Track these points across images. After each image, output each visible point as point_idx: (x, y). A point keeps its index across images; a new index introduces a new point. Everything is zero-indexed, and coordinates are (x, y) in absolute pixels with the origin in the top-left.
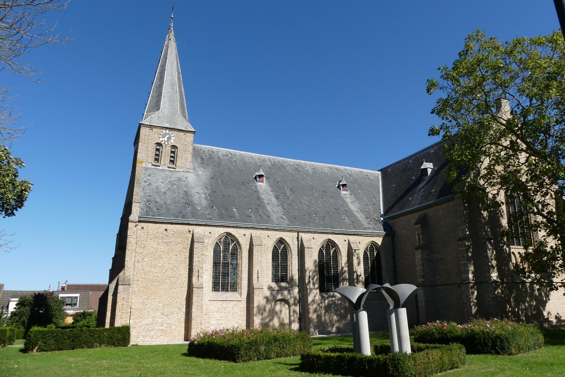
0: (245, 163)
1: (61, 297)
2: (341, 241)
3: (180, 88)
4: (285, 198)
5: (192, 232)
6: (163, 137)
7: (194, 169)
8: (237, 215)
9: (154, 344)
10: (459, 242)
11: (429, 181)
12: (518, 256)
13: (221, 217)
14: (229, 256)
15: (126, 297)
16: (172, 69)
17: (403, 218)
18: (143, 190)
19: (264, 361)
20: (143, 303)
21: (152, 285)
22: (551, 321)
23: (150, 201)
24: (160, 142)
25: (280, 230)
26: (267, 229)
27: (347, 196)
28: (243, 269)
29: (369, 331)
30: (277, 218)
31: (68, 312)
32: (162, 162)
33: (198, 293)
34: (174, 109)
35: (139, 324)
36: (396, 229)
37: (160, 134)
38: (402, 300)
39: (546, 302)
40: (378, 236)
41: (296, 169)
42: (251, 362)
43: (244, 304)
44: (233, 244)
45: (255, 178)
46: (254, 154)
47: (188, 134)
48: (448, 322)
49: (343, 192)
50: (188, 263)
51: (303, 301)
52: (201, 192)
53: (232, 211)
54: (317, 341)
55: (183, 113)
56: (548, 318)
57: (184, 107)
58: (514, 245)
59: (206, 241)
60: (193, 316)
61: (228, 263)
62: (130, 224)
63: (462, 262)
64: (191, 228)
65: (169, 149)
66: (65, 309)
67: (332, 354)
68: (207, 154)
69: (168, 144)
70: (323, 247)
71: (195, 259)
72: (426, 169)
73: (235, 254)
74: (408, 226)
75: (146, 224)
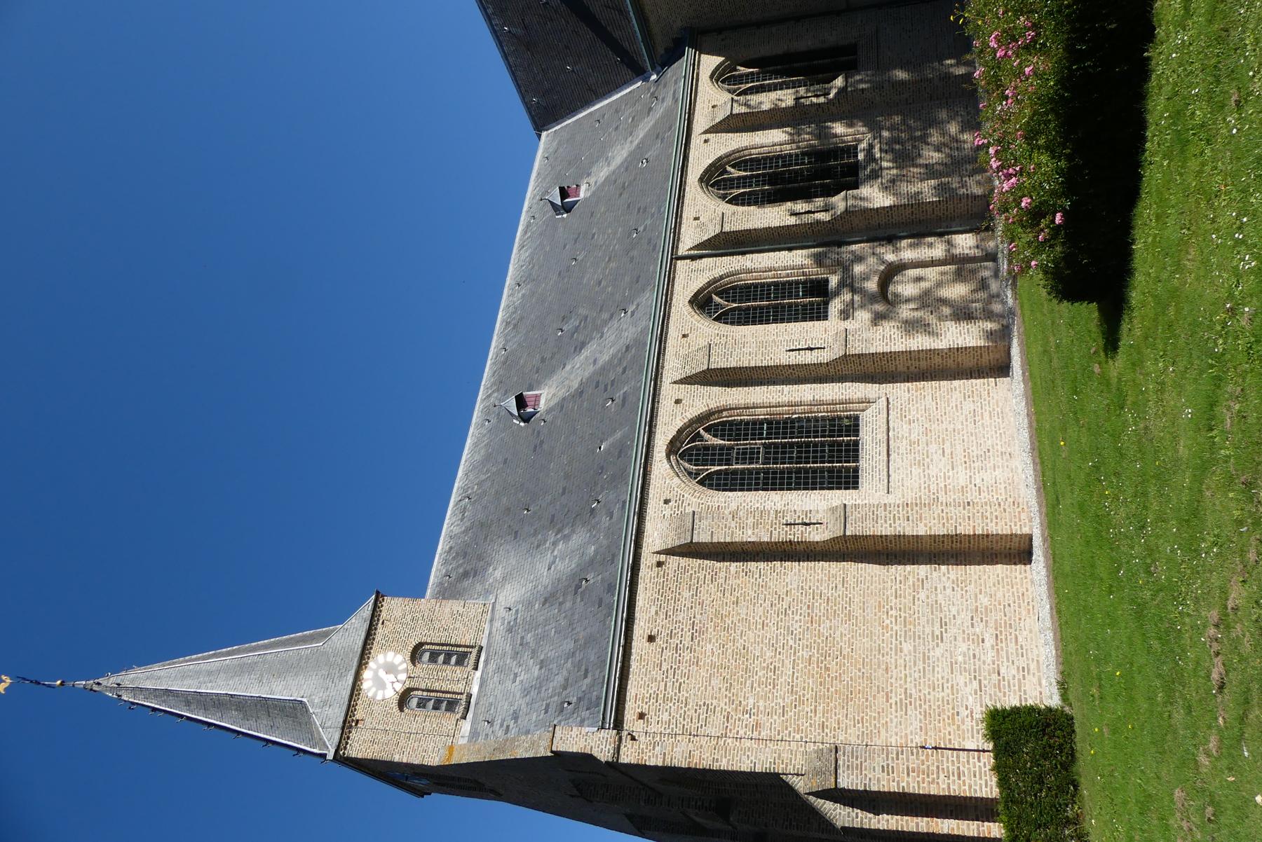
0: (488, 458)
4: (585, 327)
7: (488, 592)
8: (618, 435)
15: (880, 761)
16: (198, 673)
20: (903, 706)
21: (838, 678)
25: (668, 304)
28: (786, 400)
32: (459, 687)
40: (695, 65)
41: (515, 326)
43: (899, 391)
44: (706, 436)
47: (384, 615)
50: (762, 565)
51: (886, 228)
52: (549, 557)
53: (608, 451)
57: (311, 635)
60: (942, 531)
62: (624, 759)
64: (647, 559)
65: (424, 667)
70: (723, 197)
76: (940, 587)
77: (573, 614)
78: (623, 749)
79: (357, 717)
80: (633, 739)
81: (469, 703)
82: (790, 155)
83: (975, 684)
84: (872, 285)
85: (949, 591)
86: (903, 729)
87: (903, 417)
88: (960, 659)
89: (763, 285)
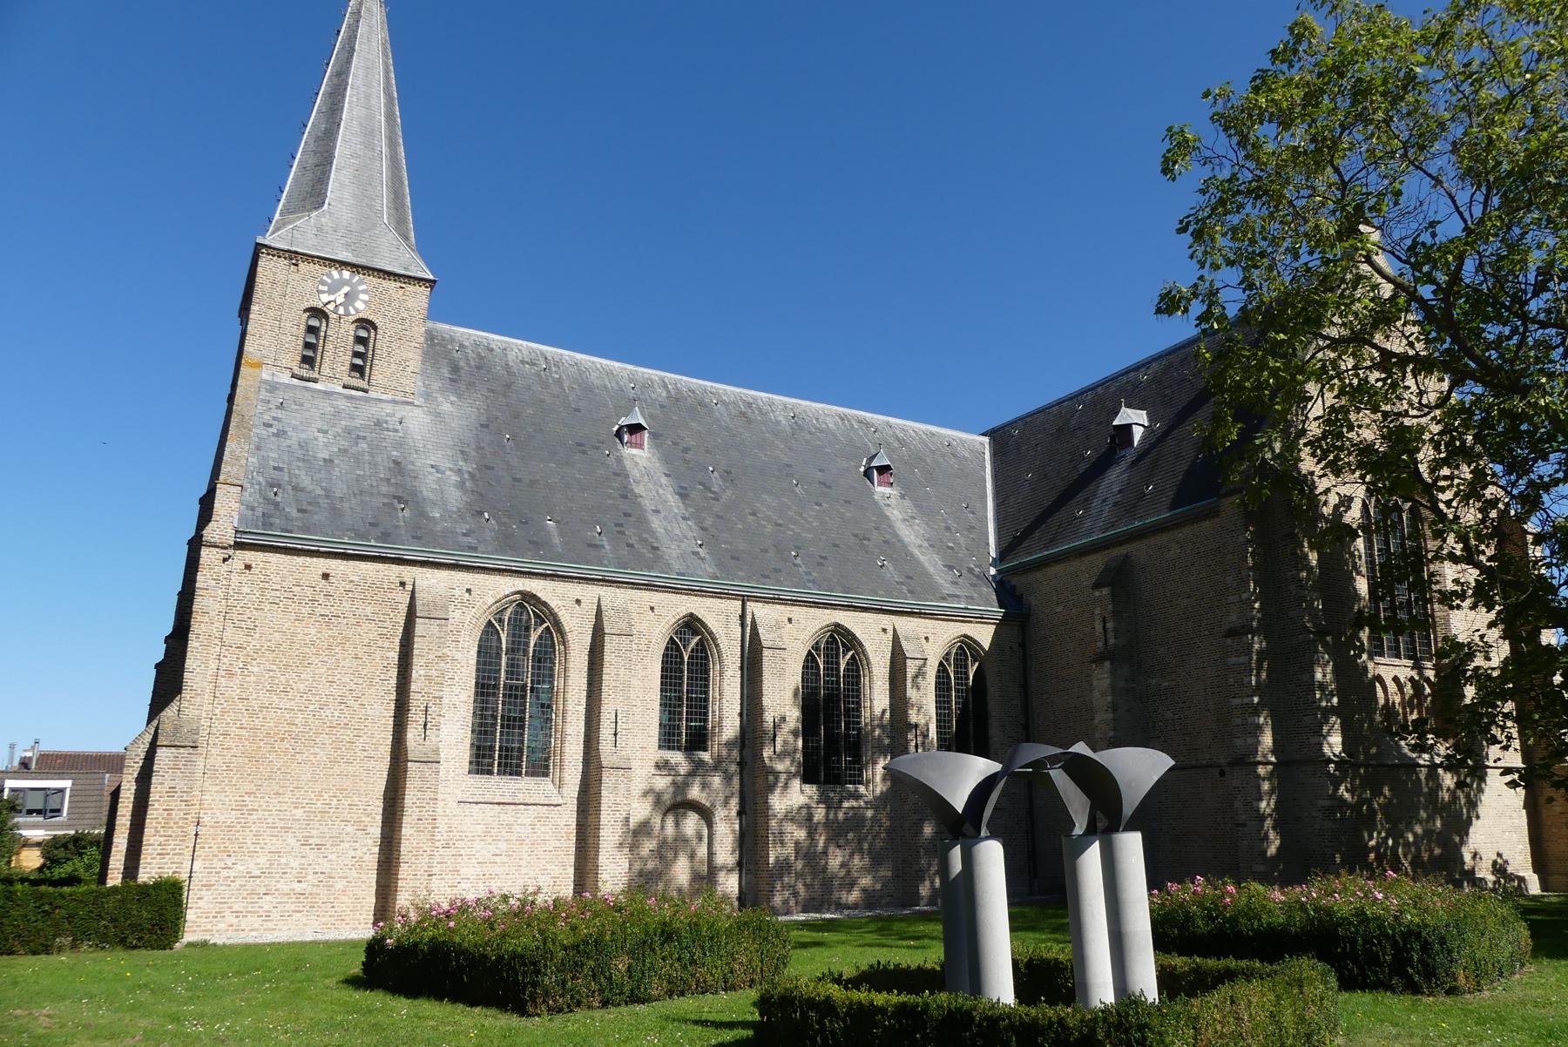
0: (588, 388)
1: (13, 790)
2: (871, 631)
3: (392, 144)
5: (409, 587)
6: (330, 292)
7: (428, 396)
8: (557, 540)
9: (269, 938)
10: (1229, 641)
11: (1134, 463)
12: (1392, 687)
13: (506, 543)
14: (528, 666)
15: (180, 785)
16: (369, 85)
17: (1056, 569)
18: (258, 448)
19: (624, 1009)
20: (240, 807)
22: (1481, 879)
23: (279, 486)
24: (320, 305)
25: (690, 592)
26: (649, 587)
27: (893, 501)
28: (570, 707)
29: (1010, 904)
30: (682, 556)
31: (25, 833)
32: (326, 370)
33: (423, 779)
34: (370, 207)
35: (225, 873)
36: (1034, 602)
37: (323, 283)
38: (1132, 797)
39: (1469, 823)
40: (981, 619)
41: (743, 414)
42: (579, 1014)
43: (568, 817)
44: (540, 630)
45: (619, 434)
46: (617, 364)
47: (410, 288)
48: (1237, 884)
49: (879, 489)
50: (394, 681)
54: (805, 933)
55: (400, 223)
56: (1472, 871)
57: (403, 205)
58: (1381, 654)
59: (455, 615)
61: (524, 686)
63: (1237, 701)
64: (408, 573)
66: (17, 826)
67: (880, 999)
68: (471, 355)
69: (347, 314)
70: (816, 647)
71: (417, 672)
72: (1127, 428)
73: (545, 659)
74: (1073, 597)
75: (260, 555)
76: (357, 845)
77: (372, 494)
78: (215, 550)
79: (301, 265)
80: (225, 560)
81: (308, 380)
82: (859, 717)
83: (257, 873)
84: (695, 793)
85: (352, 853)
86: (216, 804)
87: (539, 819)
88: (283, 860)
89: (707, 686)
